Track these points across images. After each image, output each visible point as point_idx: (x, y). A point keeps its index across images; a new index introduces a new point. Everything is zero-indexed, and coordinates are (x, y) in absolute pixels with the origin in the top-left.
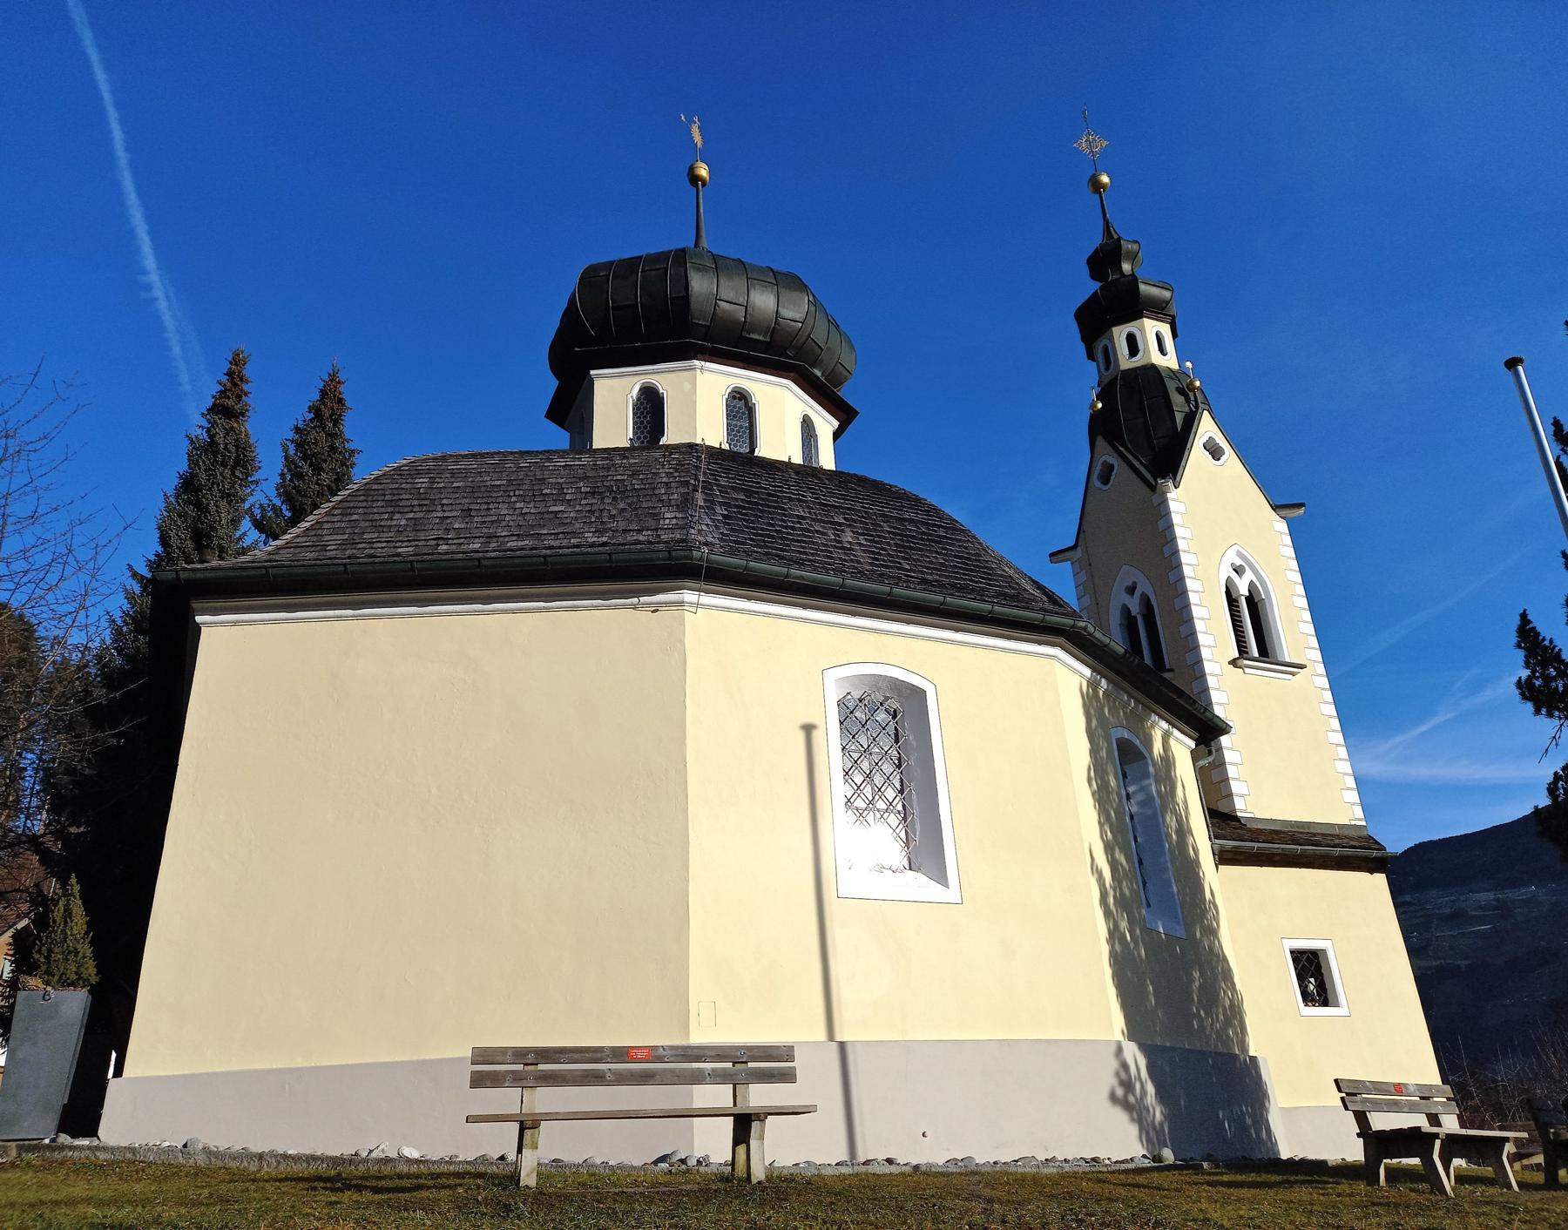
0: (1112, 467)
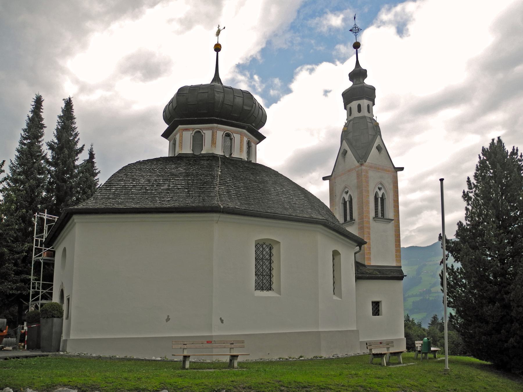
0: (346, 152)
